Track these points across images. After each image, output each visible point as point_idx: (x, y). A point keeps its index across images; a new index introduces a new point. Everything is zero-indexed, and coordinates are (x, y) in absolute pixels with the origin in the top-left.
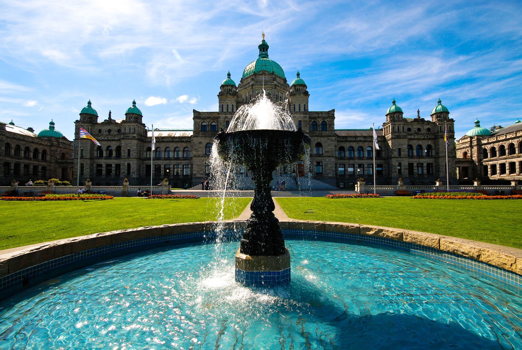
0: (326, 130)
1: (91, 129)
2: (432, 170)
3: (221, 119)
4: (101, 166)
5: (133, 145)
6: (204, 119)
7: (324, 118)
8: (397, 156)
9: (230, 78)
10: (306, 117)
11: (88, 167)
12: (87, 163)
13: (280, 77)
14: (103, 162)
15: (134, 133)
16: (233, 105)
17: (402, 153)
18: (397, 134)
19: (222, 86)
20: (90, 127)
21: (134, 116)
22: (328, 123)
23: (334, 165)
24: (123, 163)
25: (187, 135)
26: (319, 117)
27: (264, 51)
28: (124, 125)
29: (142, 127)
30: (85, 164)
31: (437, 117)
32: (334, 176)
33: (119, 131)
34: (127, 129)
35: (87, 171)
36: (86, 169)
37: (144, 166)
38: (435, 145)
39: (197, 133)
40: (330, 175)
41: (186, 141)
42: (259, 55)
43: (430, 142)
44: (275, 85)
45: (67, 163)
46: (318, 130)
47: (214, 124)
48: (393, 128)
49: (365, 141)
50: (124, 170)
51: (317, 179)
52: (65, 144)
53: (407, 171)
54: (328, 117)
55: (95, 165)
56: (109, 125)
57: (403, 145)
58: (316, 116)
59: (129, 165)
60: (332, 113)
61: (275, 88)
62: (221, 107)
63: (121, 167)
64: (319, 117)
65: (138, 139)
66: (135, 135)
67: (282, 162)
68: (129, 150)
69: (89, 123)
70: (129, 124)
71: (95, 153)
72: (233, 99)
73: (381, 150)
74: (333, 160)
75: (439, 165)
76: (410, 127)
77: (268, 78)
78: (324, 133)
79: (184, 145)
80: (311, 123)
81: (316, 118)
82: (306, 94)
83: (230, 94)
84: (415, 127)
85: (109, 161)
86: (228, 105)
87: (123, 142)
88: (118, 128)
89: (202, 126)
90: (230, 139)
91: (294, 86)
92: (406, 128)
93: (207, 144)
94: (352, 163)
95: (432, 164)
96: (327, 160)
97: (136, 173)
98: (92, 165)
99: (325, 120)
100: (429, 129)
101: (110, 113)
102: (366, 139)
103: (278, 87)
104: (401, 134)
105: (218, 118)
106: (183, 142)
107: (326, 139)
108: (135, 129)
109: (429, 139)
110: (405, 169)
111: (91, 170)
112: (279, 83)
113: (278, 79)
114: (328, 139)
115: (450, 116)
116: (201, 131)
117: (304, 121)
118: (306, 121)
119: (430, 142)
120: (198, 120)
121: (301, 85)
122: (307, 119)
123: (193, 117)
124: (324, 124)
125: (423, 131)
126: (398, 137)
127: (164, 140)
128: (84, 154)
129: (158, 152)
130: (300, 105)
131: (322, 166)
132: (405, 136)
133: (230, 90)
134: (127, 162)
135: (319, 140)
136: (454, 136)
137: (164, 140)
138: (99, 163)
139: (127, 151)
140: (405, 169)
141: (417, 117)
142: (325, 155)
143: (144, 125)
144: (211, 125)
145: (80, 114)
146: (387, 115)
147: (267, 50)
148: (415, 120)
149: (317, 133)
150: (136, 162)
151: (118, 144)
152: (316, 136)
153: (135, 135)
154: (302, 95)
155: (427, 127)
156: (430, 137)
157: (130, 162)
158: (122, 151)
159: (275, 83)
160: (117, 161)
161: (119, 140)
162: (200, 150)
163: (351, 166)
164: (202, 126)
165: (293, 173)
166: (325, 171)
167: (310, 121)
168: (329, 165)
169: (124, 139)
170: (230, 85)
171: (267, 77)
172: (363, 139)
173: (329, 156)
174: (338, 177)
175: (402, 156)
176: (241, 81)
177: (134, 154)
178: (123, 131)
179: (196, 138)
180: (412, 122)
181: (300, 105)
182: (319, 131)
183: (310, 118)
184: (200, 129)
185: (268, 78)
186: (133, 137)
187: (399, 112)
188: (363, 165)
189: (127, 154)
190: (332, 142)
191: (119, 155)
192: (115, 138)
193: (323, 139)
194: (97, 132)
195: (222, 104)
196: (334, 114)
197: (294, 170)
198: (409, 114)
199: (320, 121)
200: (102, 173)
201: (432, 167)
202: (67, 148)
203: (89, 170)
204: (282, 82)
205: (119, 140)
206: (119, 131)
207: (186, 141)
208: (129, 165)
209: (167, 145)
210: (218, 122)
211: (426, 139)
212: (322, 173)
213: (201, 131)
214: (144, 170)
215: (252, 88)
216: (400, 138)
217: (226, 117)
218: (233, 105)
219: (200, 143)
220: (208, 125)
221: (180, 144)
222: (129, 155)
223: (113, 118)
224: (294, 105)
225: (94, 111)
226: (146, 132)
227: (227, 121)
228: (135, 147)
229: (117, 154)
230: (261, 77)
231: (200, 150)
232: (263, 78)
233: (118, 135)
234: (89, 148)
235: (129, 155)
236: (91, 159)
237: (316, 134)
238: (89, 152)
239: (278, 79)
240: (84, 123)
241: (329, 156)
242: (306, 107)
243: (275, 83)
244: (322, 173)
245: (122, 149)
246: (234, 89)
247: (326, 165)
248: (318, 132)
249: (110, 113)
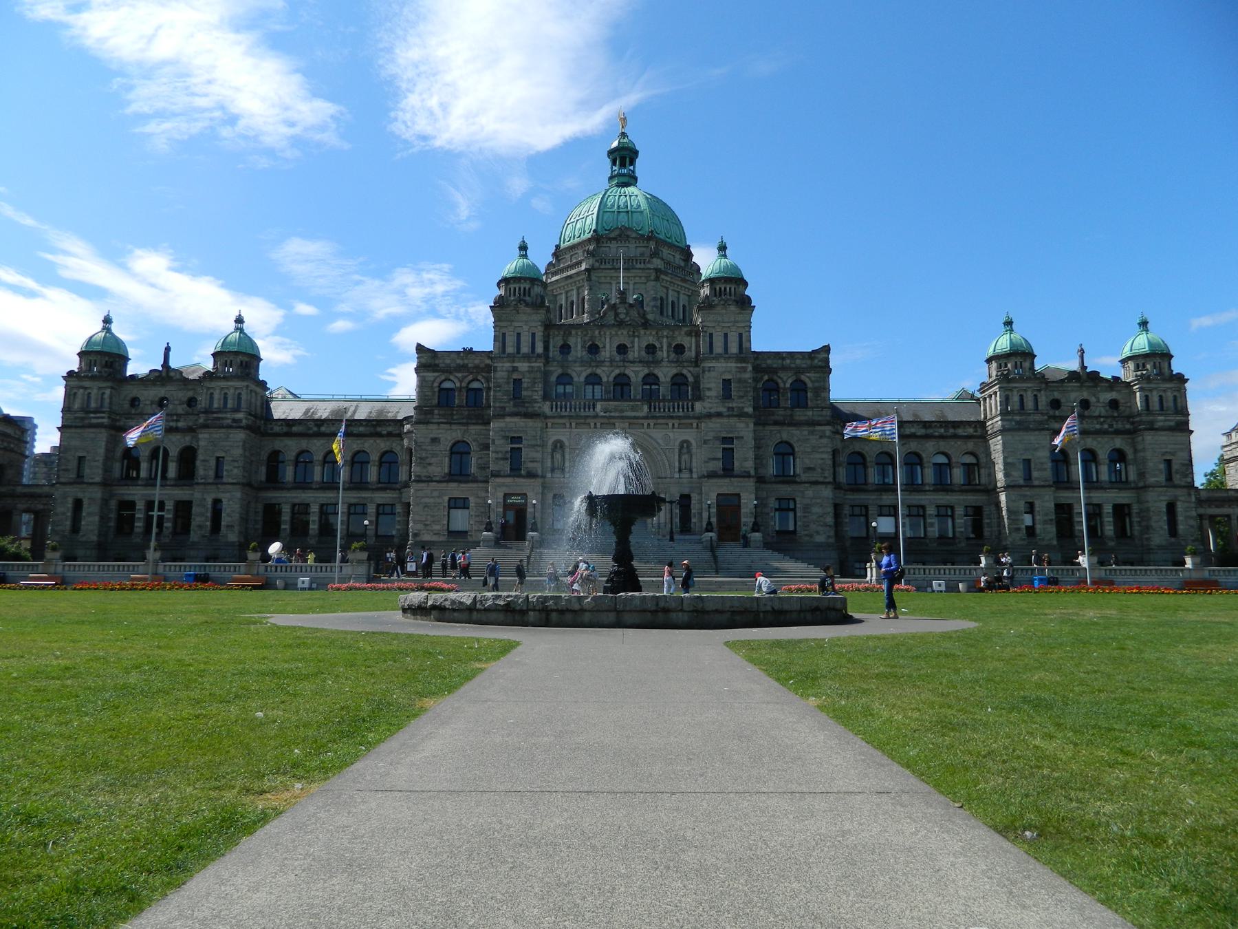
0: (806, 406)
1: (111, 397)
2: (1131, 523)
3: (499, 374)
4: (131, 505)
5: (233, 444)
6: (448, 370)
7: (799, 371)
8: (1021, 482)
9: (525, 256)
10: (744, 370)
11: (95, 509)
12: (92, 497)
13: (671, 246)
14: (138, 494)
15: (237, 410)
16: (533, 335)
17: (1035, 474)
18: (1018, 418)
19: (505, 281)
20: (108, 392)
21: (239, 359)
22: (810, 385)
23: (830, 510)
24: (202, 499)
25: (390, 416)
26: (784, 368)
27: (623, 165)
28: (207, 384)
29: (258, 390)
30: (85, 502)
31: (1137, 368)
32: (832, 540)
33: (191, 402)
34: (216, 396)
35: (90, 522)
36: (89, 514)
37: (260, 507)
38: (1136, 451)
39: (426, 413)
40: (820, 539)
41: (390, 434)
42: (611, 178)
43: (1118, 442)
44: (657, 270)
45: (13, 495)
46: (782, 404)
47: (475, 385)
48: (1006, 401)
49: (927, 437)
50: (200, 519)
51: (774, 550)
52: (8, 436)
53: (1052, 529)
54: (812, 368)
55: (113, 504)
56: (163, 385)
57: (1036, 449)
58: (776, 363)
59: (217, 502)
60: (823, 355)
61: (657, 279)
62: (500, 338)
63: (195, 510)
64: (784, 368)
65: (248, 428)
66: (240, 416)
67: (640, 440)
68: (219, 460)
69: (106, 379)
70: (223, 384)
71: (117, 466)
72: (535, 317)
73: (978, 464)
74: (827, 492)
75: (1148, 510)
76: (1057, 395)
77: (633, 249)
78: (800, 415)
79: (383, 445)
80: (760, 385)
81: (774, 371)
82: (745, 304)
83: (527, 305)
84: (1073, 395)
85: (157, 493)
86: (519, 335)
87: (204, 438)
88: (190, 394)
89: (441, 390)
90: (298, 352)
91: (712, 281)
92: (1043, 400)
93: (454, 444)
94: (888, 503)
95: (1129, 506)
96: (810, 493)
97: (236, 529)
98: (105, 502)
99: (803, 377)
100: (1114, 404)
101: (168, 350)
102: (930, 431)
103: (666, 274)
104: (1031, 418)
105: (488, 368)
106: (379, 435)
107: (805, 431)
108: (239, 398)
109: (1118, 432)
110: (1045, 522)
111: (104, 519)
112: (669, 263)
113: (665, 252)
114: (812, 433)
115: (1177, 367)
116: (439, 405)
117: (740, 381)
118: (745, 381)
119: (1118, 442)
120: (430, 375)
121: (727, 280)
122: (748, 375)
123: (415, 365)
124: (799, 388)
125: (1098, 410)
126: (1022, 427)
127: (323, 429)
128: (87, 471)
129: (301, 466)
130: (726, 335)
131: (794, 510)
132: (1040, 423)
133: (526, 292)
134: (213, 496)
135: (786, 434)
136: (1187, 423)
137: (323, 429)
138: (127, 498)
139: (213, 463)
140: (1045, 522)
141: (1074, 366)
142: (804, 477)
143: (263, 383)
144: (469, 390)
145: (81, 354)
146: (989, 361)
147: (632, 162)
148: (1073, 375)
149: (780, 413)
150: (238, 495)
151: (187, 440)
152: (776, 423)
153: (240, 416)
154: (733, 308)
155: (1107, 396)
156: (1119, 425)
157: (220, 496)
158: (198, 463)
159: (657, 263)
160: (182, 494)
161: (190, 430)
162: (433, 460)
163: (885, 510)
164: (441, 390)
165: (707, 530)
166: (806, 526)
167: (755, 380)
168: (816, 510)
169: (205, 426)
170: (525, 279)
171: (632, 246)
172: (921, 431)
173: (816, 483)
174: (848, 543)
175: (1036, 483)
176: (555, 255)
177: (233, 472)
178: (203, 401)
179: (421, 426)
180: (1062, 381)
181: (726, 335)
182: (786, 408)
183: (756, 369)
184: (435, 401)
185: (633, 249)
186: (234, 420)
187: (1021, 355)
188: (923, 507)
189: (212, 473)
190: (825, 441)
191: (187, 472)
192: (180, 424)
193: (795, 432)
194: (127, 406)
195: (504, 330)
196: (827, 361)
197: (709, 523)
198: (1054, 358)
199: (786, 380)
200: (132, 527)
201: (1129, 515)
202: (12, 451)
203: (97, 518)
204: (678, 259)
205: (190, 430)
206: (191, 402)
207: (390, 434)
208: (217, 502)
209: (304, 444)
210: (488, 380)
211: (1105, 432)
212: (794, 532)
213: (439, 405)
214: (260, 518)
215: (589, 279)
216: (1027, 429)
217: (515, 369)
218: (533, 335)
219: (435, 440)
220: (460, 389)
221: (371, 441)
222: (218, 475)
223: (173, 364)
224: (711, 335)
225: (119, 343)
226: (266, 404)
227: (515, 380)
228: (237, 452)
229: (180, 470)
230: (613, 245)
231: (433, 460)
232: (619, 251)
233: (187, 414)
234: (102, 451)
235: (218, 475)
236: (106, 484)
237: (776, 418)
238: (100, 464)
239: (665, 252)
240: (93, 378)
241: (816, 483)
242: (744, 338)
243: (657, 263)
244: (794, 532)
245: (200, 457)
246: (537, 289)
247: (806, 508)
248: (781, 412)
249: (168, 350)
